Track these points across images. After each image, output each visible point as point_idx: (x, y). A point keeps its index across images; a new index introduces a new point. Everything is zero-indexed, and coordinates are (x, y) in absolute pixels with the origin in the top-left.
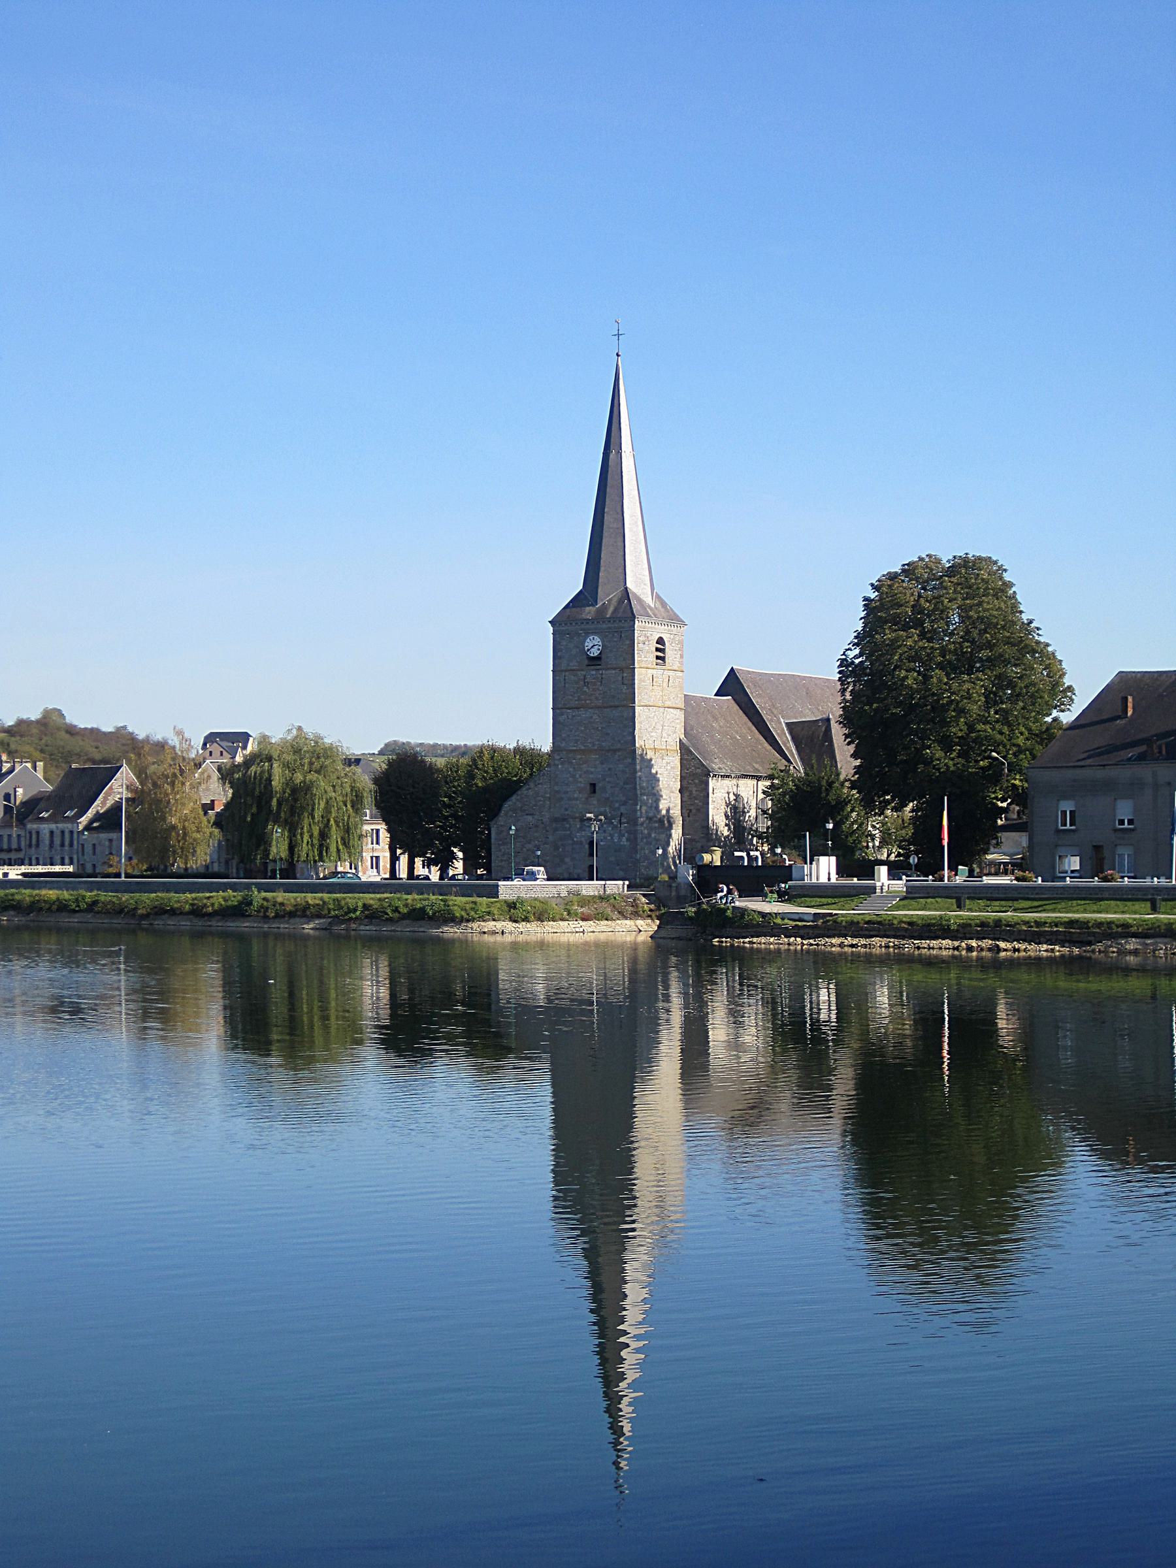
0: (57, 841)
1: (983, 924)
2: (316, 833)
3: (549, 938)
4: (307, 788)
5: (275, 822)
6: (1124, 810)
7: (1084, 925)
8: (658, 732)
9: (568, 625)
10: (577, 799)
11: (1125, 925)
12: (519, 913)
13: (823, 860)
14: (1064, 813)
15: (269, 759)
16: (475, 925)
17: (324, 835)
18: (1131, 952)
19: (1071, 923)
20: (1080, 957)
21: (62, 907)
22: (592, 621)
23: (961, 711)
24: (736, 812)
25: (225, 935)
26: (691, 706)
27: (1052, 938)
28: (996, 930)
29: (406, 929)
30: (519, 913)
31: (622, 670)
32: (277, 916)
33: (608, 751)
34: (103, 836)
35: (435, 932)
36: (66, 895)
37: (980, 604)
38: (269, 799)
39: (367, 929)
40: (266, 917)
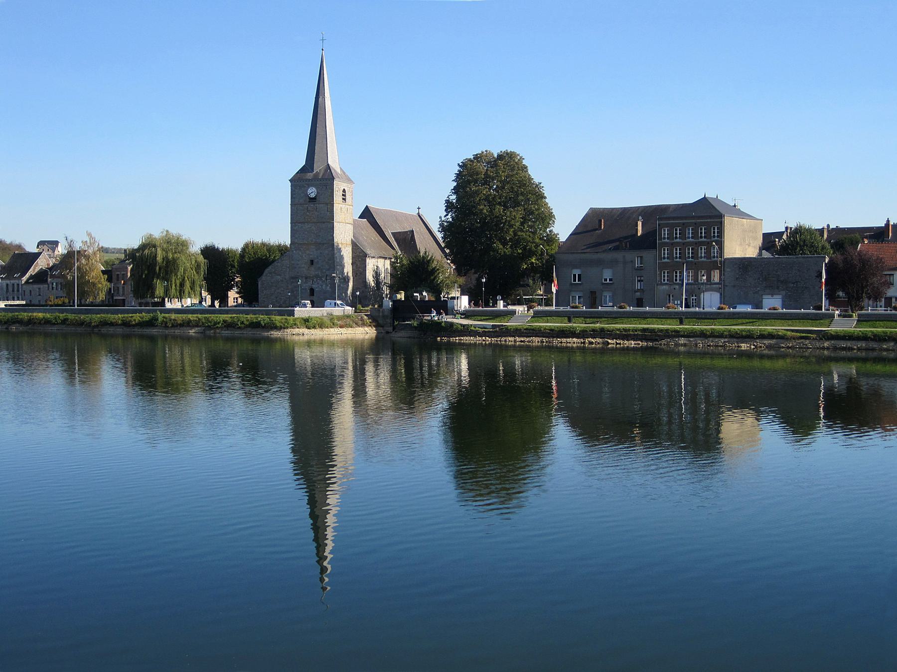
0: (10, 289)
1: (593, 330)
2: (178, 282)
3: (326, 337)
4: (174, 260)
5: (158, 278)
6: (607, 274)
7: (652, 331)
8: (344, 234)
9: (299, 182)
11: (676, 331)
12: (310, 324)
14: (575, 276)
15: (155, 246)
16: (289, 330)
17: (182, 285)
18: (682, 345)
19: (644, 330)
20: (652, 348)
21: (47, 322)
22: (312, 180)
23: (511, 226)
24: (377, 274)
25: (142, 337)
27: (635, 338)
28: (601, 333)
29: (249, 333)
30: (310, 324)
31: (327, 204)
32: (173, 326)
34: (36, 286)
35: (266, 334)
36: (48, 315)
37: (517, 174)
38: (148, 267)
39: (226, 333)
40: (166, 327)
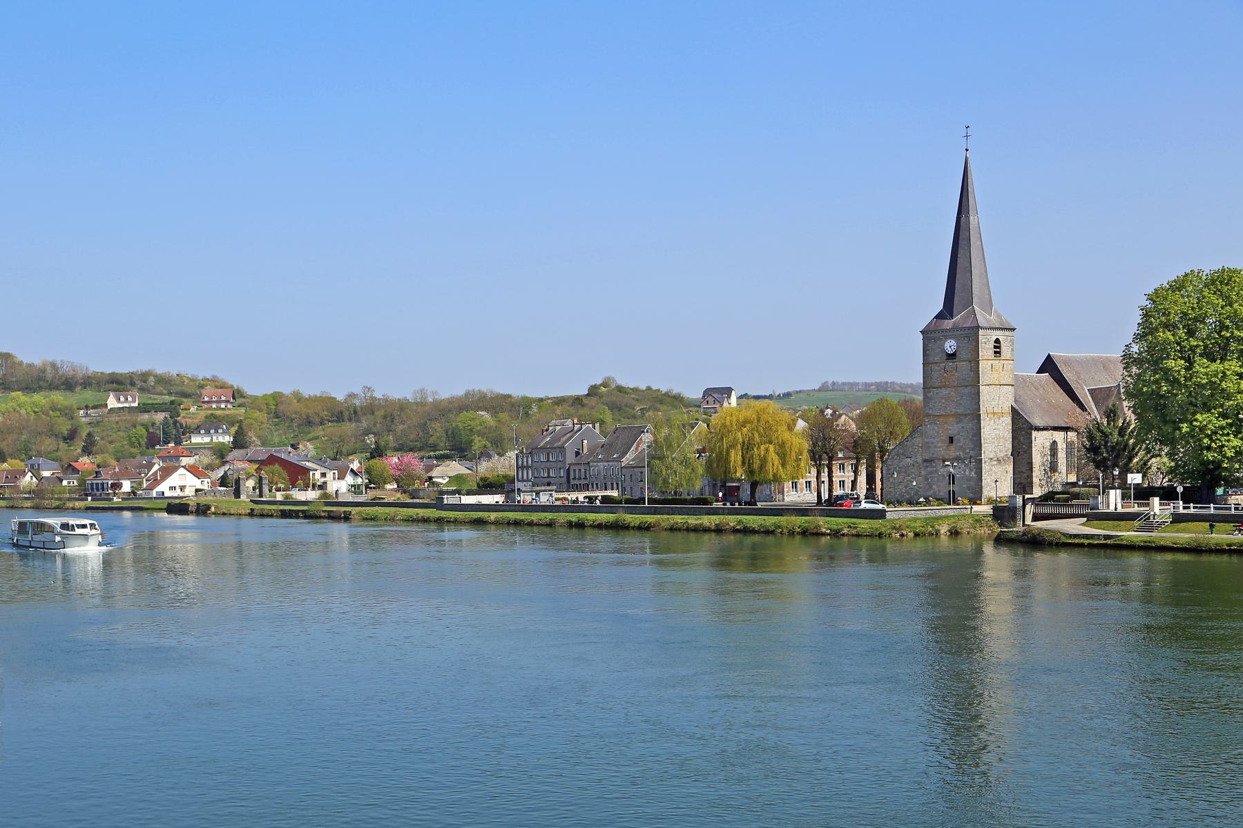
13: (1112, 492)
26: (1018, 383)
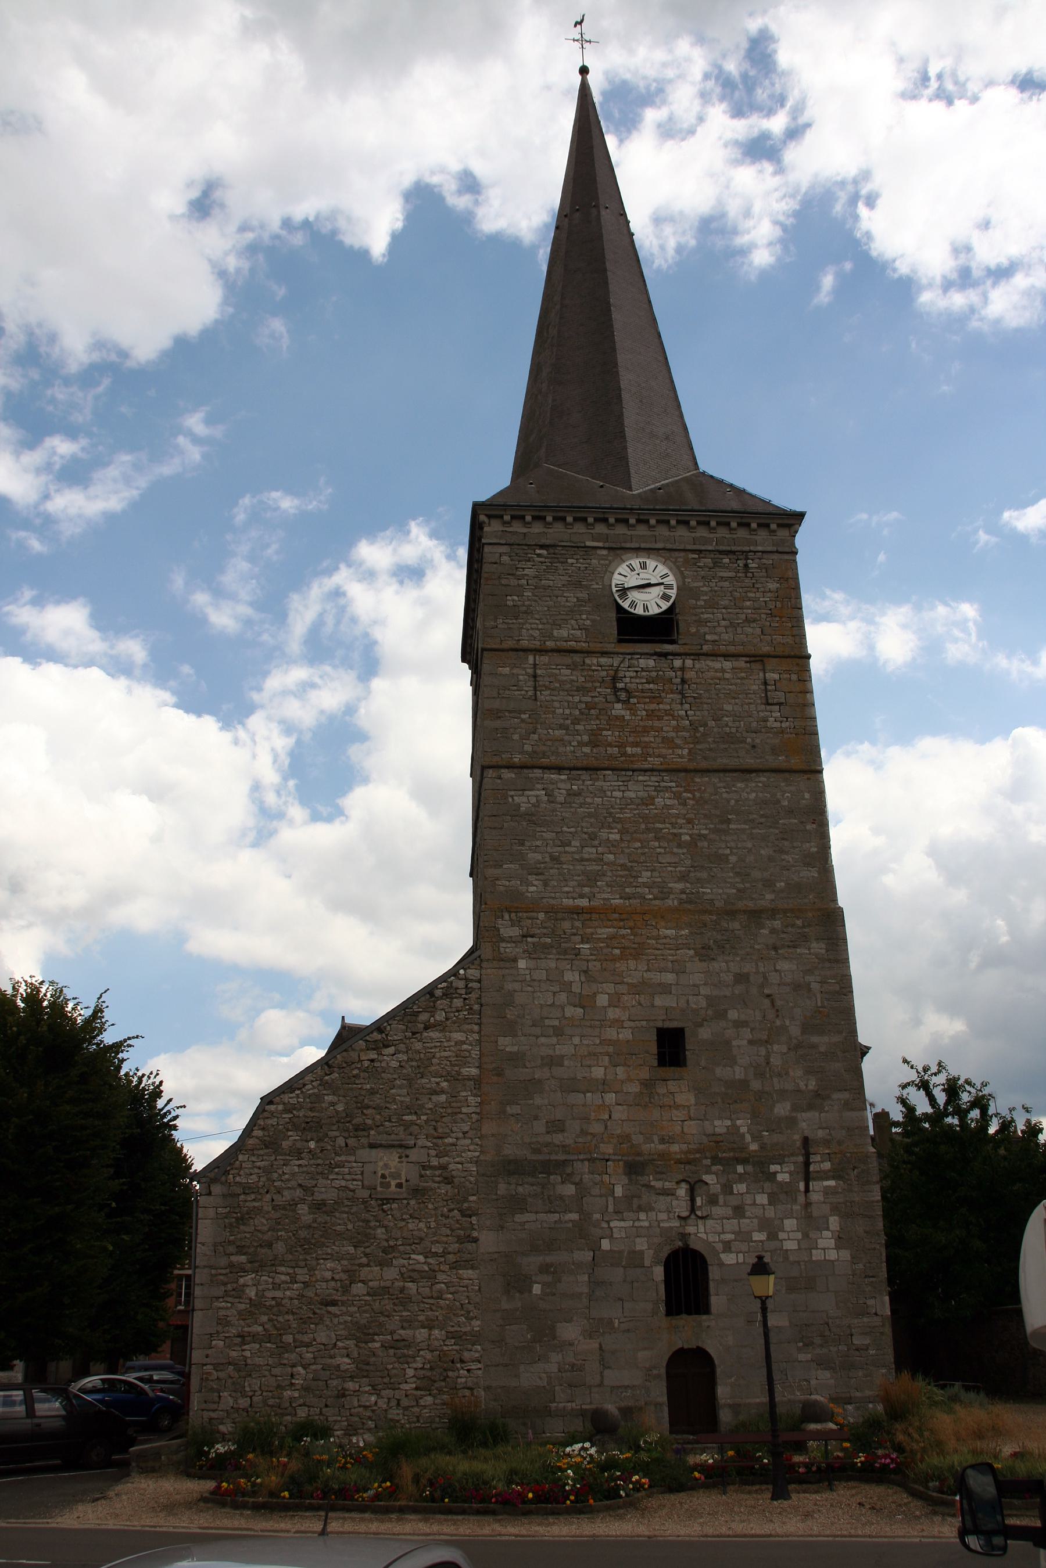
10: (604, 1086)
33: (732, 914)
